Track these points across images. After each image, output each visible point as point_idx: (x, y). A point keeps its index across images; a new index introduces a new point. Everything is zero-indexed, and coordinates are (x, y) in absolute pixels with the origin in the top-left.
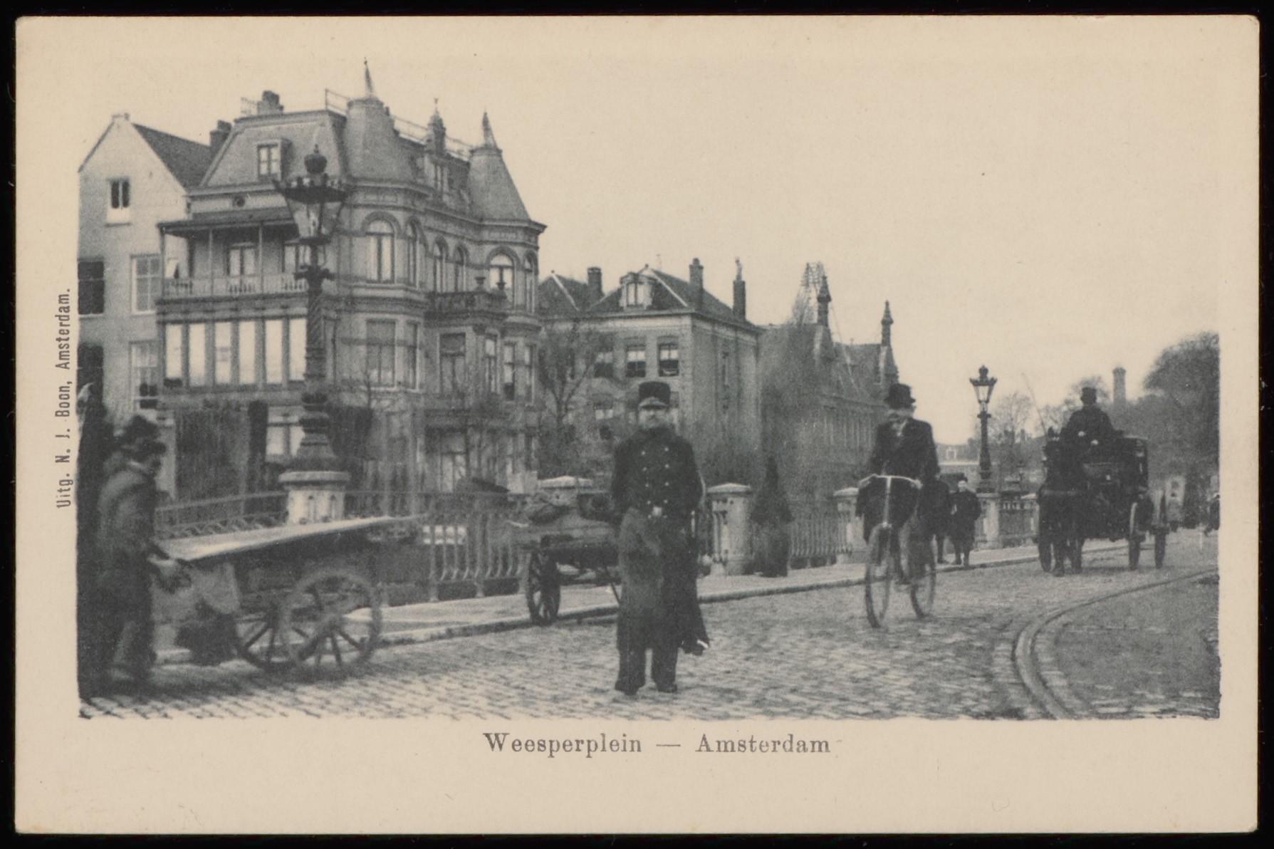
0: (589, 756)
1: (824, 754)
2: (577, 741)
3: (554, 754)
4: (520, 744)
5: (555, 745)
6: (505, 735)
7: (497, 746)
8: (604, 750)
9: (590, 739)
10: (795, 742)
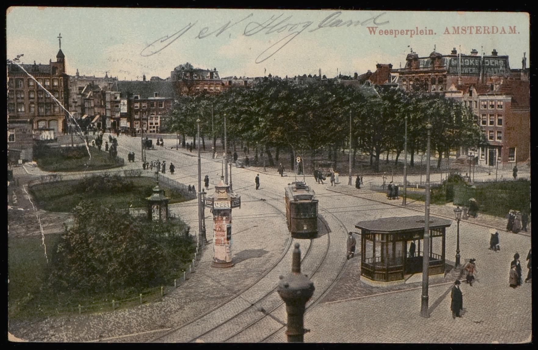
3: (397, 36)
4: (382, 32)
5: (397, 32)
7: (373, 33)
9: (396, 29)
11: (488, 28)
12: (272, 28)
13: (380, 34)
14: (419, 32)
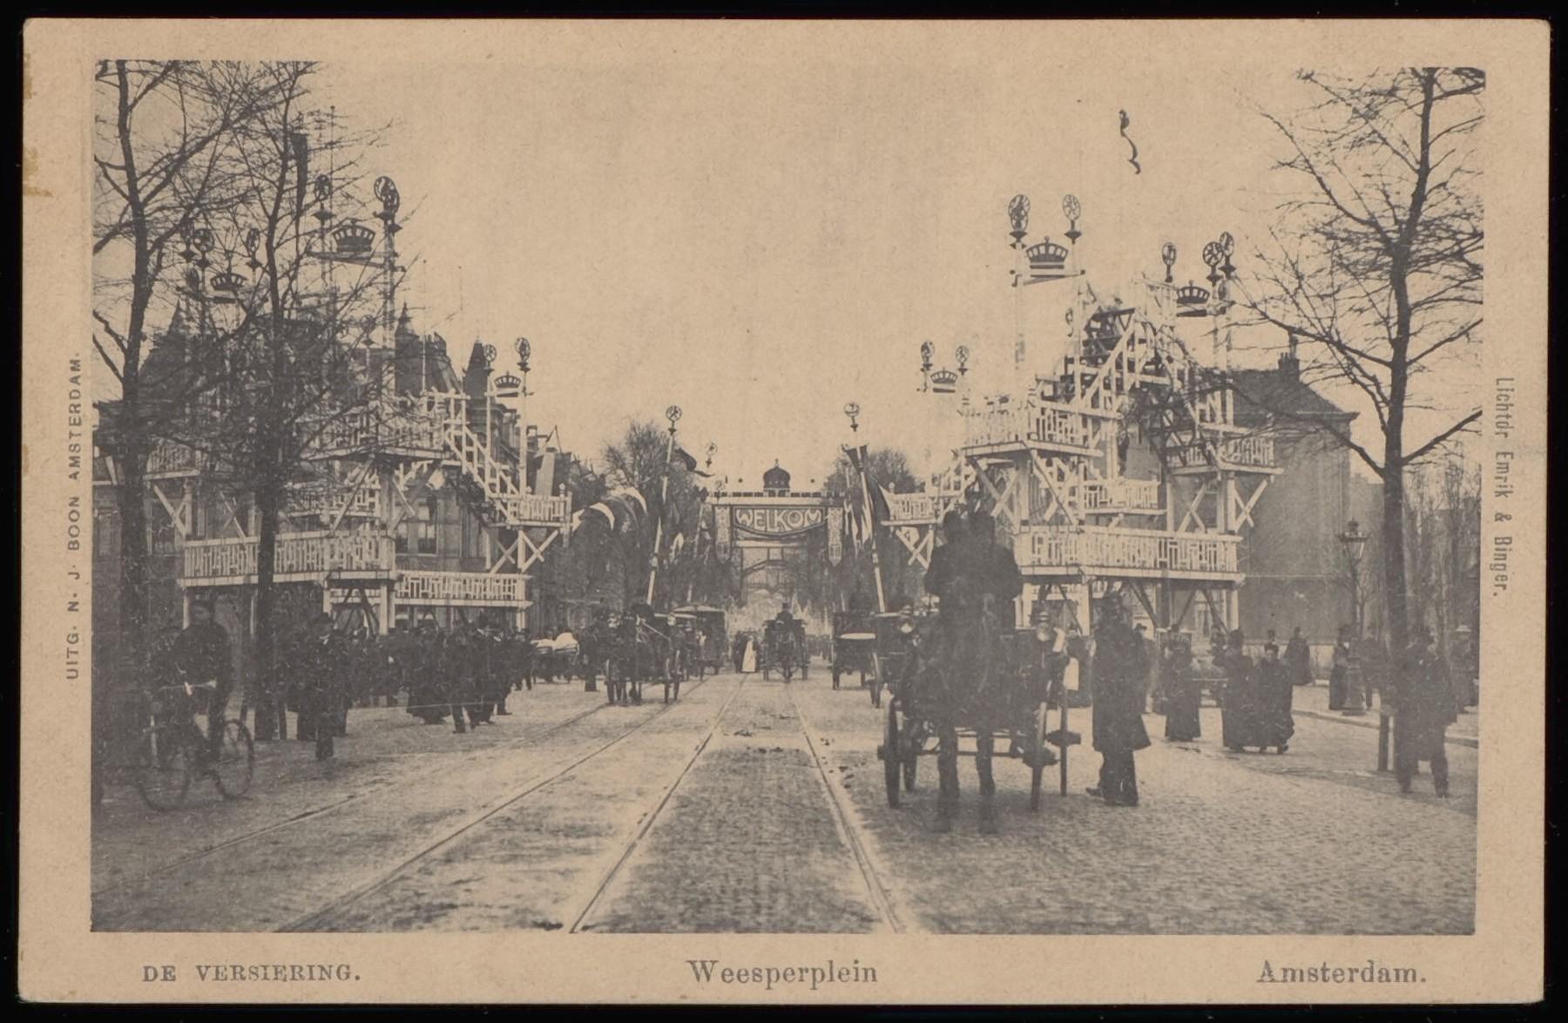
0: (769, 988)
1: (870, 982)
2: (801, 970)
4: (747, 974)
5: (774, 974)
6: (713, 962)
8: (832, 980)
10: (1376, 971)
11: (242, 969)
12: (572, 723)
13: (724, 980)
14: (836, 975)
